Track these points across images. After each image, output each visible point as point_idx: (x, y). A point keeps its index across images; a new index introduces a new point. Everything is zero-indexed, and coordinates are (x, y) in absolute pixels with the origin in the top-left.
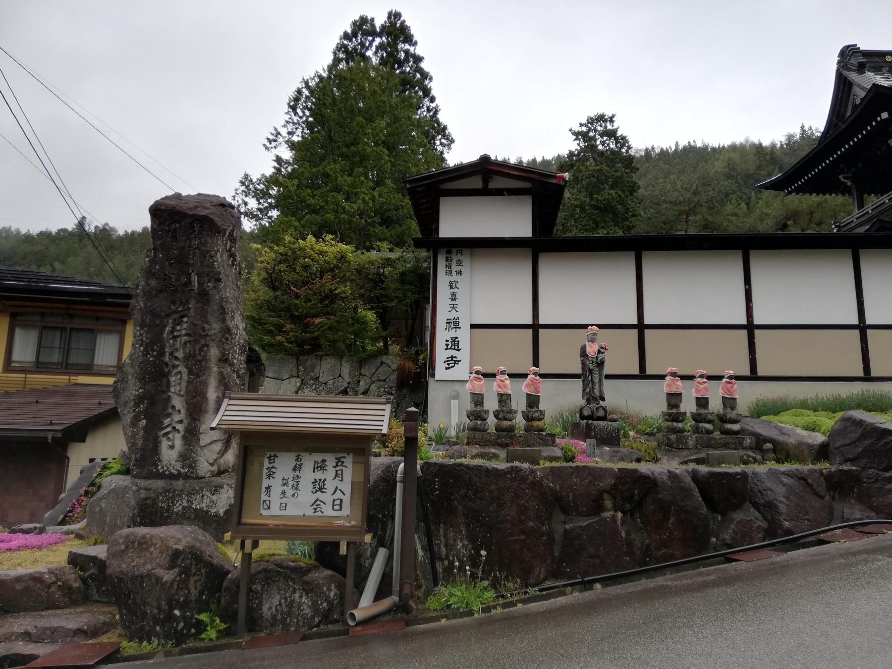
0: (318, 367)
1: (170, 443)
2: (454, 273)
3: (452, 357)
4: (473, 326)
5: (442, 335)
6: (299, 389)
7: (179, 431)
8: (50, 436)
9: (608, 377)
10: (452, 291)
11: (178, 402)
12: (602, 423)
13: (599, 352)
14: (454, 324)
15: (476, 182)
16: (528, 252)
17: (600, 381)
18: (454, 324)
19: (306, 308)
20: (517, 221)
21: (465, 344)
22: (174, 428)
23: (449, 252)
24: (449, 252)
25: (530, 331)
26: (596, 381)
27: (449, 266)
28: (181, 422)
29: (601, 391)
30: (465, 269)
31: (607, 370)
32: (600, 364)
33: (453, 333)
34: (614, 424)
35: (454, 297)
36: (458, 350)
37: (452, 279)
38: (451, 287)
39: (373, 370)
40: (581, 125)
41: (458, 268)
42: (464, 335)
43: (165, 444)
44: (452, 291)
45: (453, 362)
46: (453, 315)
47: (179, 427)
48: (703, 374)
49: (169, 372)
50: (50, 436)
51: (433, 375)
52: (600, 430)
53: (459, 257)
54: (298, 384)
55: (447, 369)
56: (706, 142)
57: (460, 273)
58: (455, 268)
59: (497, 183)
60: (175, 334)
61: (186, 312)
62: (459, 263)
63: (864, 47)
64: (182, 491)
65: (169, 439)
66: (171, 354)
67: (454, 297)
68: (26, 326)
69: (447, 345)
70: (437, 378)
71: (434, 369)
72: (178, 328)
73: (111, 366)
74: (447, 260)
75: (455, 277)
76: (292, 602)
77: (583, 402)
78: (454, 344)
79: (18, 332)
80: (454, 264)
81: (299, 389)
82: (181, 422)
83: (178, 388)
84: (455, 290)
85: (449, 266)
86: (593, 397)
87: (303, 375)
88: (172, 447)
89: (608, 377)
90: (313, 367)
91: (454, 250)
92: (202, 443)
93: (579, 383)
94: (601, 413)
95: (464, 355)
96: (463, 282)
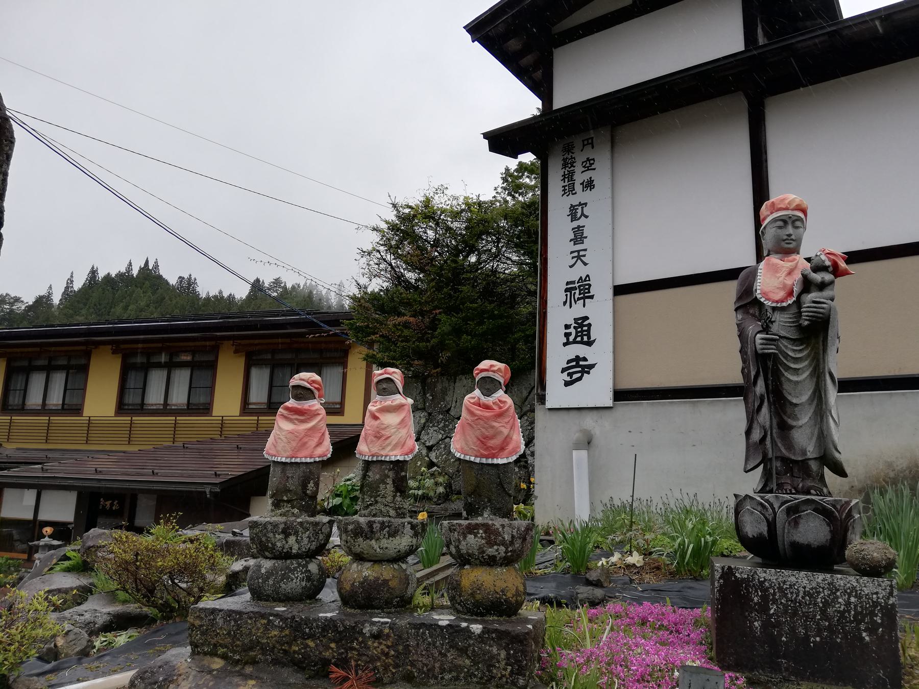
0: (450, 393)
2: (578, 188)
3: (577, 359)
4: (620, 290)
5: (559, 316)
6: (423, 428)
8: (208, 491)
9: (847, 386)
10: (575, 224)
11: (91, 466)
12: (802, 580)
13: (807, 285)
14: (580, 290)
17: (819, 396)
18: (580, 290)
19: (420, 303)
21: (602, 331)
24: (569, 149)
26: (800, 396)
27: (569, 177)
29: (823, 437)
30: (601, 175)
31: (843, 361)
32: (815, 331)
34: (869, 586)
35: (578, 236)
36: (589, 343)
37: (574, 200)
38: (574, 217)
39: (525, 393)
42: (600, 311)
44: (575, 224)
45: (578, 369)
46: (580, 271)
48: (500, 585)
50: (208, 491)
51: (542, 399)
52: (793, 610)
53: (589, 153)
54: (423, 421)
55: (567, 384)
57: (589, 185)
58: (580, 177)
62: (589, 165)
64: (465, 538)
67: (578, 236)
68: (260, 364)
69: (567, 335)
70: (549, 405)
71: (543, 388)
73: (336, 403)
74: (565, 166)
77: (750, 484)
78: (581, 331)
79: (254, 372)
80: (578, 168)
81: (423, 428)
85: (569, 177)
86: (787, 464)
87: (430, 406)
89: (847, 386)
90: (444, 392)
93: (734, 413)
94: (813, 531)
95: (600, 353)
96: (596, 202)
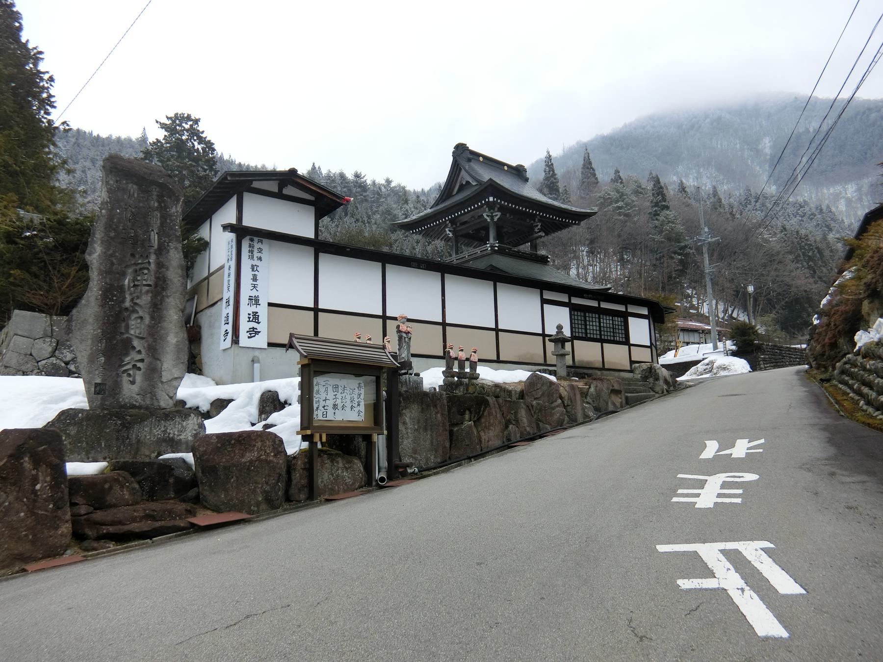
1: (131, 379)
2: (255, 258)
3: (253, 328)
4: (270, 305)
7: (139, 369)
15: (273, 186)
16: (311, 250)
18: (255, 301)
20: (301, 223)
22: (134, 366)
23: (252, 240)
25: (312, 313)
27: (251, 252)
28: (142, 360)
33: (254, 309)
35: (255, 278)
36: (259, 323)
38: (253, 270)
40: (168, 118)
41: (259, 255)
42: (263, 311)
43: (125, 379)
45: (253, 332)
46: (254, 293)
47: (139, 365)
49: (129, 317)
56: (233, 158)
57: (260, 259)
58: (256, 254)
59: (289, 191)
60: (136, 283)
61: (147, 266)
62: (260, 250)
63: (472, 147)
65: (129, 375)
66: (132, 300)
67: (255, 278)
70: (241, 345)
72: (139, 278)
74: (250, 246)
75: (256, 262)
76: (338, 476)
78: (255, 317)
80: (256, 251)
82: (142, 360)
83: (138, 331)
84: (256, 273)
85: (251, 252)
88: (133, 383)
91: (256, 239)
92: (164, 379)
95: (263, 327)
